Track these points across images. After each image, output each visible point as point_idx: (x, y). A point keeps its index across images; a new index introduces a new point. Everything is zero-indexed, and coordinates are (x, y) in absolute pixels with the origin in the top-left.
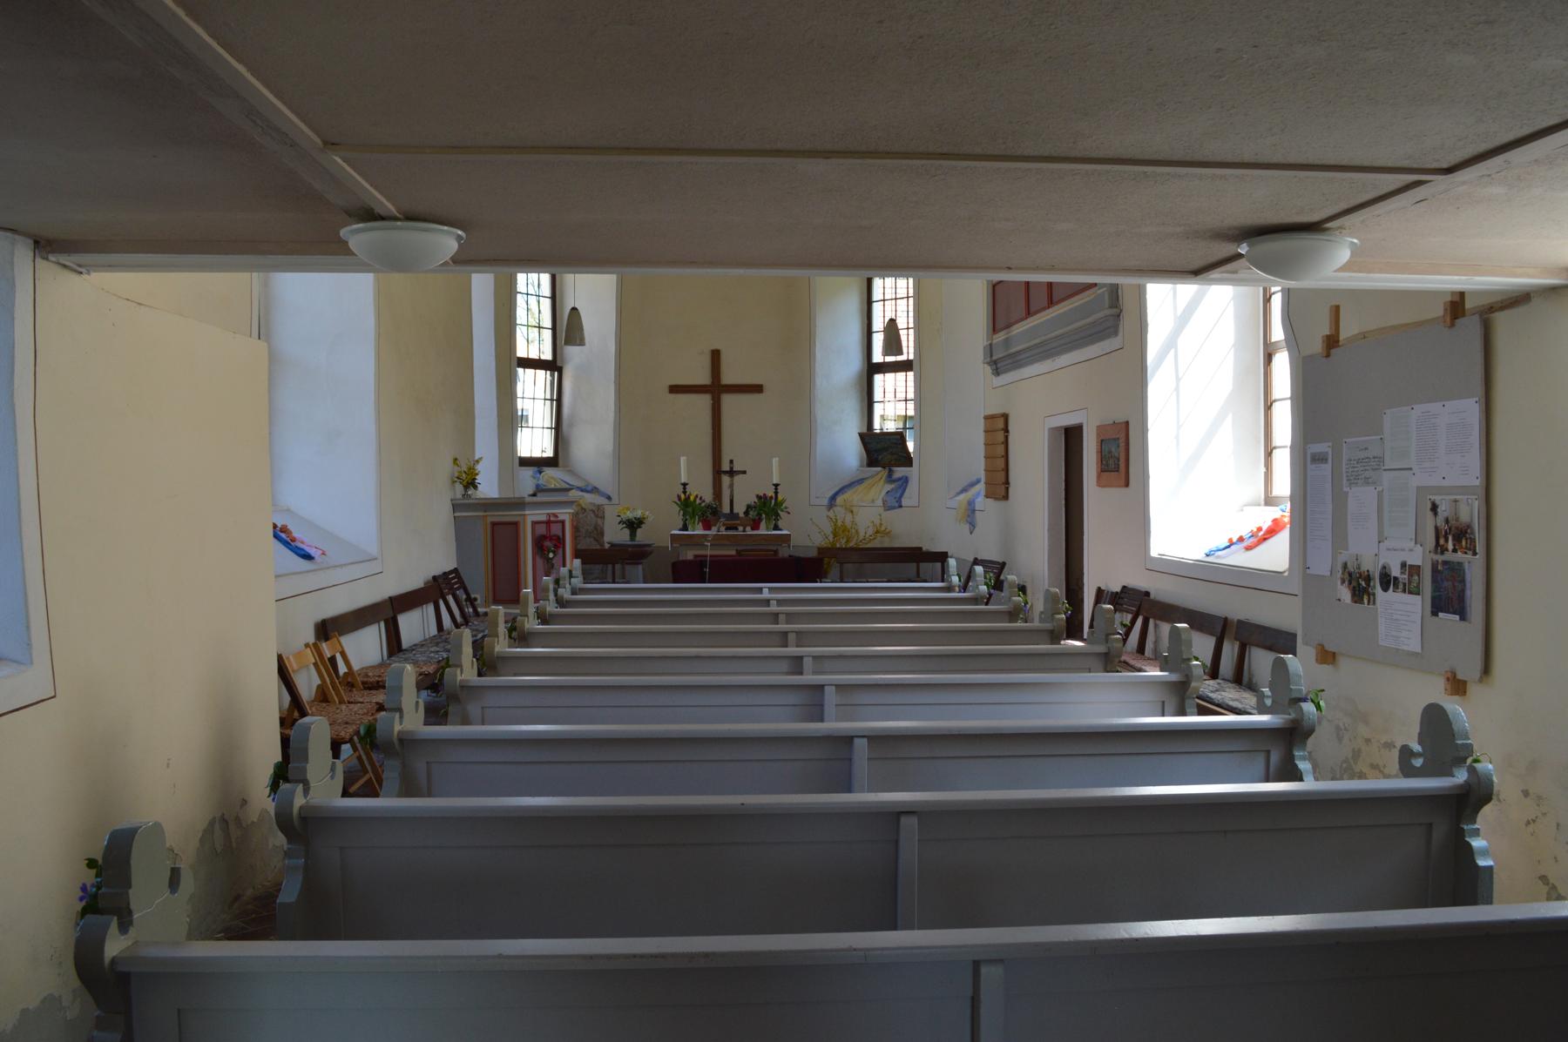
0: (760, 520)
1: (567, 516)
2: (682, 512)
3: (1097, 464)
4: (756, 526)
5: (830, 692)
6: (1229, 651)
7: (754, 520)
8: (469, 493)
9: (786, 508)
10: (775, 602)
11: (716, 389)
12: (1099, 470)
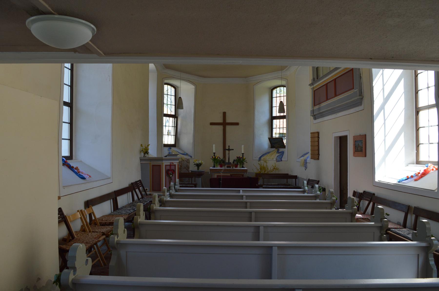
0: (238, 165)
1: (177, 163)
2: (213, 162)
3: (353, 148)
4: (236, 167)
5: (275, 250)
6: (411, 218)
7: (236, 165)
8: (145, 155)
9: (246, 161)
10: (245, 196)
11: (224, 124)
12: (354, 151)
